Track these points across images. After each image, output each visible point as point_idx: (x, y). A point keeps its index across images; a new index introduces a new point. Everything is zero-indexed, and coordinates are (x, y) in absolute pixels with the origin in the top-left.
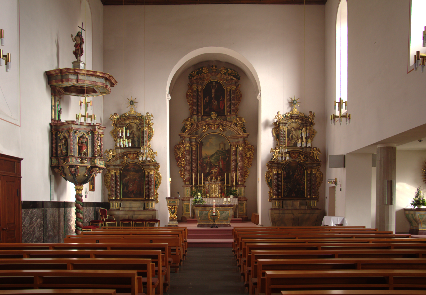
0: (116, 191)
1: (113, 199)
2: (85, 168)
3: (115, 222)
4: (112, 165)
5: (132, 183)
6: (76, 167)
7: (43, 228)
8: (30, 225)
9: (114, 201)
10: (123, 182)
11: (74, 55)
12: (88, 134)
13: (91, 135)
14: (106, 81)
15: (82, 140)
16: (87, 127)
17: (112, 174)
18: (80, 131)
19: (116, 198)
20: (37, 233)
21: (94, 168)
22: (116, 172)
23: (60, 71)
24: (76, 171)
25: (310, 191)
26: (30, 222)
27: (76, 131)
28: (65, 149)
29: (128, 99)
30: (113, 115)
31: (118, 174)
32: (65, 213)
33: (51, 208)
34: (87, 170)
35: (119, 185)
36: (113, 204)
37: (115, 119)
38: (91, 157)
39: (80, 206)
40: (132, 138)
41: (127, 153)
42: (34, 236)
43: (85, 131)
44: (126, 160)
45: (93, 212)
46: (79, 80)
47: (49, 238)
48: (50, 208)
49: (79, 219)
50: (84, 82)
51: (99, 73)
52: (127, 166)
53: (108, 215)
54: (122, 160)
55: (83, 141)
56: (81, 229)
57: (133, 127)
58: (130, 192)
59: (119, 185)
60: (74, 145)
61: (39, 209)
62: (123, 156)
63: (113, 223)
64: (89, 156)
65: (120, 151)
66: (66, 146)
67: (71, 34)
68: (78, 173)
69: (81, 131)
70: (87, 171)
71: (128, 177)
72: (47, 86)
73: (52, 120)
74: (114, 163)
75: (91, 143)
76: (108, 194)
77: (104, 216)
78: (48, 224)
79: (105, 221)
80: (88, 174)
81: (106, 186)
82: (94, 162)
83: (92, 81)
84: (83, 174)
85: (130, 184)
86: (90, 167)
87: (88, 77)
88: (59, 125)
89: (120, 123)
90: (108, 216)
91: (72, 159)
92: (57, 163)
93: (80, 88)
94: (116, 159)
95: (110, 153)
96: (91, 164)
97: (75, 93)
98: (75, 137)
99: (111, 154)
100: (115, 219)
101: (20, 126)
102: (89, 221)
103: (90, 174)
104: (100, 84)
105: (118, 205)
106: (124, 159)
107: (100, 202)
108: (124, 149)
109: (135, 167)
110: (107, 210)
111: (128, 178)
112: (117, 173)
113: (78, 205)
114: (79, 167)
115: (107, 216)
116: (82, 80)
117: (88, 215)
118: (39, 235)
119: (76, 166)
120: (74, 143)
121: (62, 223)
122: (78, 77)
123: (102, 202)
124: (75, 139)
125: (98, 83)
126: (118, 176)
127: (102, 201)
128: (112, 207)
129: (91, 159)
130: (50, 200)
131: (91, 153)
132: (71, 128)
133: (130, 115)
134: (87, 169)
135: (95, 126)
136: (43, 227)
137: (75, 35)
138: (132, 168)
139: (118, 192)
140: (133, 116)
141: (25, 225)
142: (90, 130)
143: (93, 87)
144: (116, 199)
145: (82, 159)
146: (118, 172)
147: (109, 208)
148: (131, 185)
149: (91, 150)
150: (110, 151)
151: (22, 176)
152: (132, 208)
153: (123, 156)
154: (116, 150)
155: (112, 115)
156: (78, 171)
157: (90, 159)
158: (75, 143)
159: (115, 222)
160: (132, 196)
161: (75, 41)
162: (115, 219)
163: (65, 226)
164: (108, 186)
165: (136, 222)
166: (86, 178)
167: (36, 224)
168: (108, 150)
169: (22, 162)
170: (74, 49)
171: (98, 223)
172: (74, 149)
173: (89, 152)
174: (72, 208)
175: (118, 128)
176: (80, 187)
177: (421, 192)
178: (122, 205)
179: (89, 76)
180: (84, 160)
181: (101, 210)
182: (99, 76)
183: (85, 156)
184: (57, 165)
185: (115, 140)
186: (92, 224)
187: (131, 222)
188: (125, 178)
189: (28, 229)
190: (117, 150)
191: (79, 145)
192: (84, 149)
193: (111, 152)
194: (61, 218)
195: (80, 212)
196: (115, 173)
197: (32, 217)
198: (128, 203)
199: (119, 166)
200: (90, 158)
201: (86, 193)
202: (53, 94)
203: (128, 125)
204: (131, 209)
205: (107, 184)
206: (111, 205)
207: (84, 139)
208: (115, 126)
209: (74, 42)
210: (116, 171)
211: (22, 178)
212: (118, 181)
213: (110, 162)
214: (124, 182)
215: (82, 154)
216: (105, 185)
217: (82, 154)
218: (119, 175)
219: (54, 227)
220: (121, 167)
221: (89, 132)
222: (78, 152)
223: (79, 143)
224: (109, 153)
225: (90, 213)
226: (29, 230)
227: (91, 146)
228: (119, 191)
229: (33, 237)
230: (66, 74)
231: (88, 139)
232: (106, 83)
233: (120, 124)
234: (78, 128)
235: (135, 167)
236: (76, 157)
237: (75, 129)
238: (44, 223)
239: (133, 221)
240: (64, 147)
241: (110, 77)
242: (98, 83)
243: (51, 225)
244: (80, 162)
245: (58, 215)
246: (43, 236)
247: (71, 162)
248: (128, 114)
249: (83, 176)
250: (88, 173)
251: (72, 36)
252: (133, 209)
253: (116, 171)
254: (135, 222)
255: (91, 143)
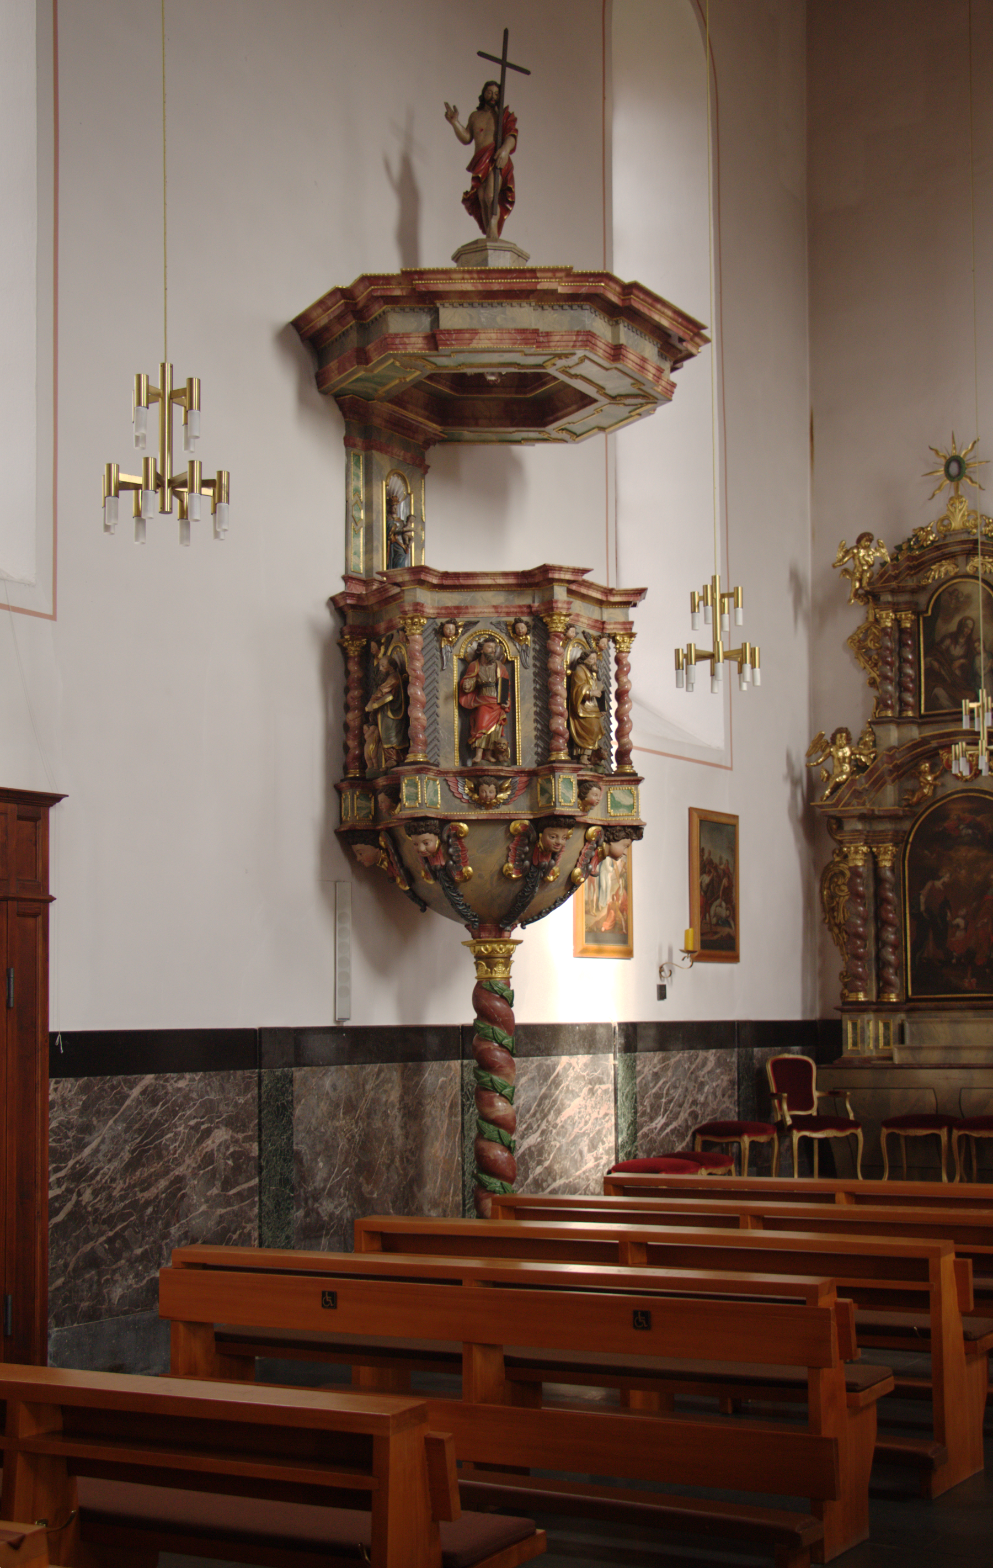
0: (878, 957)
1: (858, 1003)
2: (500, 832)
3: (848, 1133)
4: (853, 817)
5: (963, 912)
6: (447, 828)
7: (260, 1181)
8: (131, 1166)
9: (864, 1011)
10: (918, 903)
11: (472, 219)
12: (514, 634)
13: (534, 642)
14: (617, 323)
15: (477, 676)
16: (511, 597)
17: (857, 867)
18: (468, 625)
19: (878, 996)
20: (203, 1213)
21: (547, 830)
22: (879, 854)
23: (346, 304)
24: (451, 850)
25: (880, 901)
26: (132, 1152)
27: (442, 625)
28: (394, 734)
29: (933, 453)
30: (855, 544)
31: (888, 864)
32: (462, 1090)
33: (333, 1068)
34: (511, 846)
35: (892, 925)
36: (859, 1031)
37: (862, 565)
38: (533, 766)
39: (498, 1054)
40: (962, 661)
41: (934, 744)
42: (173, 1230)
43: (499, 623)
44: (928, 782)
45: (726, 1078)
46: (442, 332)
47: (321, 1236)
48: (330, 1064)
49: (492, 1127)
50: (471, 340)
51: (550, 275)
52: (940, 815)
53: (817, 1089)
54: (909, 785)
55: (484, 679)
56: (499, 1184)
57: (968, 597)
58: (954, 961)
59: (897, 921)
60: (430, 706)
61: (224, 1073)
62: (916, 760)
63: (835, 1137)
64: (520, 761)
65: (899, 739)
66: (400, 717)
67: (447, 105)
68: (465, 865)
69: (475, 623)
70: (515, 849)
71: (946, 878)
72: (303, 399)
73: (347, 579)
74: (864, 804)
75: (535, 689)
76: (841, 974)
77: (785, 1095)
78: (307, 1158)
79: (791, 1128)
80: (520, 869)
81: (831, 930)
82: (547, 795)
83: (519, 327)
84: (497, 868)
85: (957, 916)
86: (527, 822)
87: (495, 310)
88: (372, 601)
89: (894, 584)
90: (819, 1098)
91: (416, 787)
92: (364, 812)
93: (517, 393)
94: (878, 784)
95: (837, 750)
96: (533, 807)
97: (494, 426)
98: (439, 661)
99: (844, 758)
100: (852, 1116)
101: (53, 617)
102: (688, 1127)
103: (536, 864)
104: (565, 338)
105: (891, 1034)
106: (918, 778)
107: (796, 1016)
108: (920, 725)
109: (979, 819)
110: (817, 1063)
111: (944, 884)
112: (881, 857)
113: (485, 1046)
114: (465, 826)
115: (816, 1094)
116: (459, 331)
117: (677, 1094)
118: (219, 1223)
119: (444, 822)
120: (432, 694)
121: (437, 1144)
122: (435, 321)
123: (809, 1017)
124: (438, 669)
125: (557, 338)
126: (888, 874)
127: (804, 1012)
128: (855, 1044)
129: (535, 778)
130: (330, 1023)
131: (537, 745)
132: (411, 608)
133: (947, 533)
134: (510, 836)
135: (552, 588)
136: (260, 1173)
137: (468, 106)
138: (962, 827)
139: (887, 964)
140: (964, 537)
141: (87, 1168)
142: (525, 610)
143: (540, 366)
144: (877, 1003)
145: (476, 777)
146: (885, 853)
147: (840, 1052)
148: (960, 921)
149: (536, 729)
150: (838, 743)
151: (52, 892)
152: (957, 1048)
153: (916, 760)
154: (873, 733)
155: (848, 547)
156: (464, 849)
157: (525, 779)
158: (442, 695)
159: (848, 1133)
160: (966, 984)
161: (472, 138)
162: (855, 1116)
163: (463, 1160)
164: (839, 929)
165: (967, 1133)
166: (517, 887)
167: (190, 1162)
168: (828, 738)
169: (55, 814)
170: (465, 182)
171: (737, 1139)
172: (435, 730)
173: (524, 738)
174: (426, 1064)
175: (884, 614)
176: (495, 946)
177: (495, 1156)
178: (912, 1034)
179: (501, 304)
180: (485, 786)
181: (777, 1065)
182: (554, 292)
183: (498, 762)
184: (361, 825)
185: (874, 678)
186: (706, 1145)
187: (943, 1133)
188: (929, 885)
189: (116, 1193)
190: (879, 730)
191: (463, 700)
192: (484, 725)
193: (841, 747)
194: (427, 1120)
195: (495, 1090)
196: (873, 858)
197: (157, 1124)
198: (942, 1022)
199: (893, 817)
200: (532, 774)
201: (661, 976)
202: (359, 441)
203: (941, 590)
204: (952, 1057)
205: (834, 918)
206: (850, 1035)
207: (492, 666)
208: (871, 604)
209: (466, 143)
210: (878, 848)
211: (53, 907)
212: (887, 901)
213: (839, 801)
214: (922, 908)
215: (480, 753)
216: (827, 926)
217: (480, 753)
218: (892, 869)
219: (365, 1168)
220: (906, 825)
221: (518, 621)
222: (457, 740)
223: (461, 690)
224: (830, 754)
225: (702, 1085)
226: (123, 1198)
227: (535, 705)
228: (892, 958)
229: (165, 1236)
230: (377, 310)
231: (517, 664)
232: (616, 335)
233: (893, 592)
234: (457, 608)
235: (979, 819)
236: (441, 773)
237: (439, 615)
238: (265, 1154)
239: (951, 1122)
240: (391, 723)
241: (631, 293)
242: (557, 338)
243: (338, 1160)
244: (468, 802)
245: (402, 1099)
246: (260, 1227)
247: (412, 805)
248: (939, 532)
249: (499, 879)
250: (523, 861)
251: (451, 115)
252: (967, 1057)
253: (874, 850)
254: (961, 1133)
255: (533, 686)
